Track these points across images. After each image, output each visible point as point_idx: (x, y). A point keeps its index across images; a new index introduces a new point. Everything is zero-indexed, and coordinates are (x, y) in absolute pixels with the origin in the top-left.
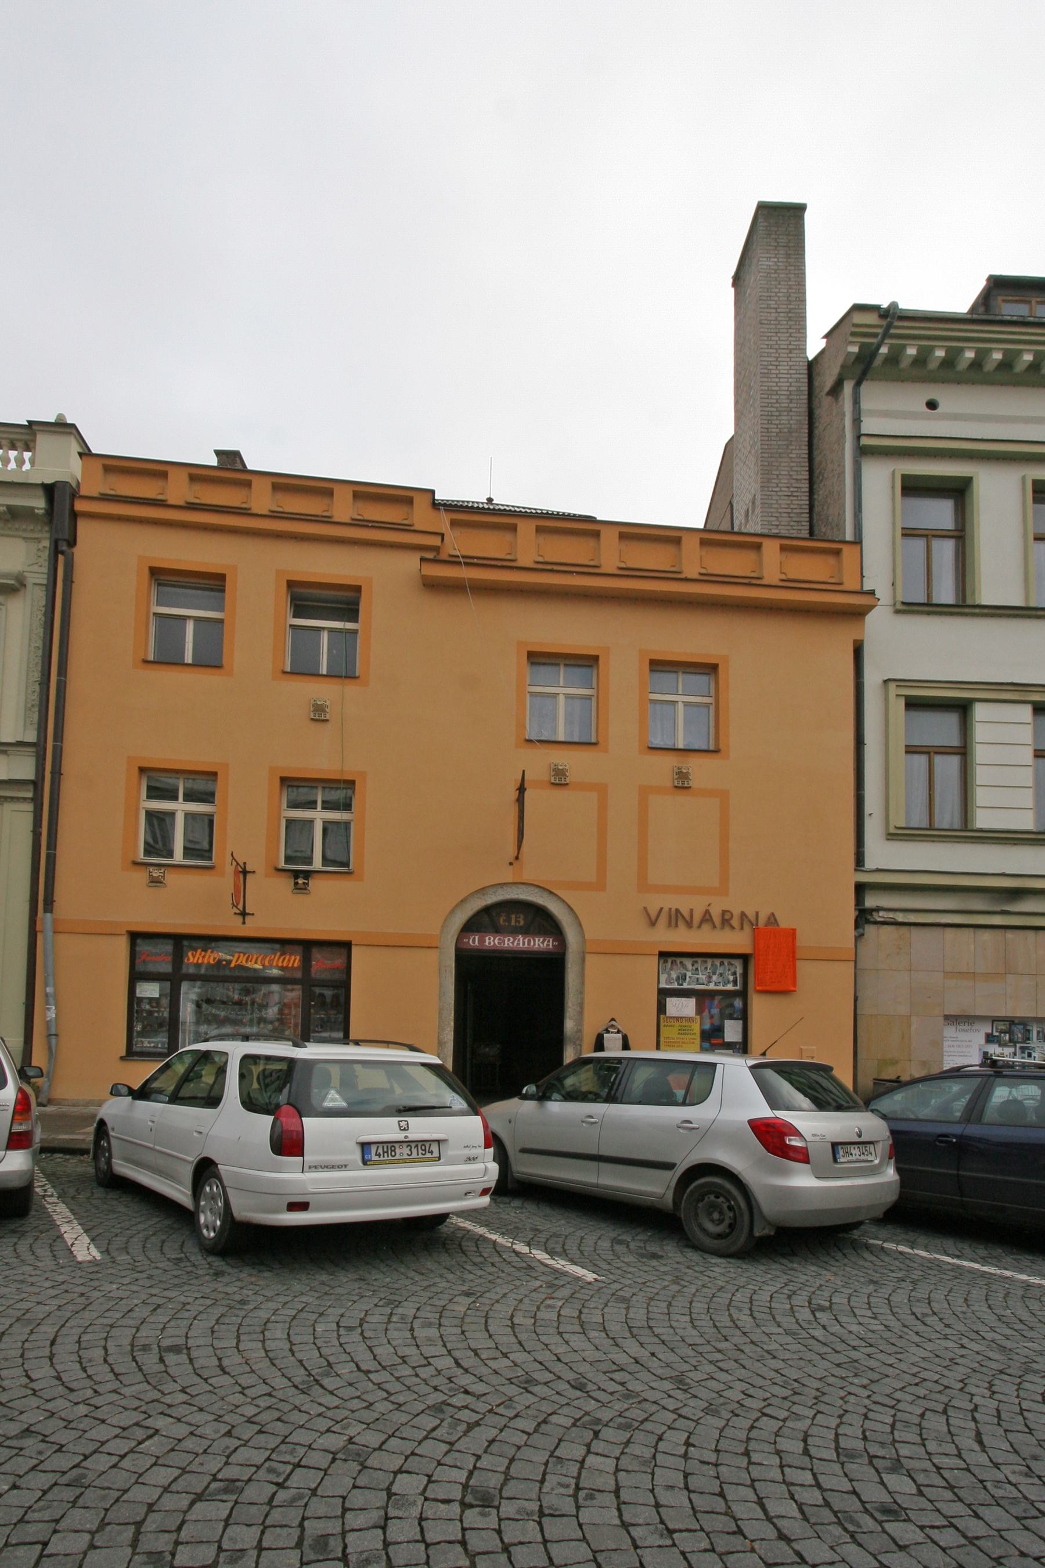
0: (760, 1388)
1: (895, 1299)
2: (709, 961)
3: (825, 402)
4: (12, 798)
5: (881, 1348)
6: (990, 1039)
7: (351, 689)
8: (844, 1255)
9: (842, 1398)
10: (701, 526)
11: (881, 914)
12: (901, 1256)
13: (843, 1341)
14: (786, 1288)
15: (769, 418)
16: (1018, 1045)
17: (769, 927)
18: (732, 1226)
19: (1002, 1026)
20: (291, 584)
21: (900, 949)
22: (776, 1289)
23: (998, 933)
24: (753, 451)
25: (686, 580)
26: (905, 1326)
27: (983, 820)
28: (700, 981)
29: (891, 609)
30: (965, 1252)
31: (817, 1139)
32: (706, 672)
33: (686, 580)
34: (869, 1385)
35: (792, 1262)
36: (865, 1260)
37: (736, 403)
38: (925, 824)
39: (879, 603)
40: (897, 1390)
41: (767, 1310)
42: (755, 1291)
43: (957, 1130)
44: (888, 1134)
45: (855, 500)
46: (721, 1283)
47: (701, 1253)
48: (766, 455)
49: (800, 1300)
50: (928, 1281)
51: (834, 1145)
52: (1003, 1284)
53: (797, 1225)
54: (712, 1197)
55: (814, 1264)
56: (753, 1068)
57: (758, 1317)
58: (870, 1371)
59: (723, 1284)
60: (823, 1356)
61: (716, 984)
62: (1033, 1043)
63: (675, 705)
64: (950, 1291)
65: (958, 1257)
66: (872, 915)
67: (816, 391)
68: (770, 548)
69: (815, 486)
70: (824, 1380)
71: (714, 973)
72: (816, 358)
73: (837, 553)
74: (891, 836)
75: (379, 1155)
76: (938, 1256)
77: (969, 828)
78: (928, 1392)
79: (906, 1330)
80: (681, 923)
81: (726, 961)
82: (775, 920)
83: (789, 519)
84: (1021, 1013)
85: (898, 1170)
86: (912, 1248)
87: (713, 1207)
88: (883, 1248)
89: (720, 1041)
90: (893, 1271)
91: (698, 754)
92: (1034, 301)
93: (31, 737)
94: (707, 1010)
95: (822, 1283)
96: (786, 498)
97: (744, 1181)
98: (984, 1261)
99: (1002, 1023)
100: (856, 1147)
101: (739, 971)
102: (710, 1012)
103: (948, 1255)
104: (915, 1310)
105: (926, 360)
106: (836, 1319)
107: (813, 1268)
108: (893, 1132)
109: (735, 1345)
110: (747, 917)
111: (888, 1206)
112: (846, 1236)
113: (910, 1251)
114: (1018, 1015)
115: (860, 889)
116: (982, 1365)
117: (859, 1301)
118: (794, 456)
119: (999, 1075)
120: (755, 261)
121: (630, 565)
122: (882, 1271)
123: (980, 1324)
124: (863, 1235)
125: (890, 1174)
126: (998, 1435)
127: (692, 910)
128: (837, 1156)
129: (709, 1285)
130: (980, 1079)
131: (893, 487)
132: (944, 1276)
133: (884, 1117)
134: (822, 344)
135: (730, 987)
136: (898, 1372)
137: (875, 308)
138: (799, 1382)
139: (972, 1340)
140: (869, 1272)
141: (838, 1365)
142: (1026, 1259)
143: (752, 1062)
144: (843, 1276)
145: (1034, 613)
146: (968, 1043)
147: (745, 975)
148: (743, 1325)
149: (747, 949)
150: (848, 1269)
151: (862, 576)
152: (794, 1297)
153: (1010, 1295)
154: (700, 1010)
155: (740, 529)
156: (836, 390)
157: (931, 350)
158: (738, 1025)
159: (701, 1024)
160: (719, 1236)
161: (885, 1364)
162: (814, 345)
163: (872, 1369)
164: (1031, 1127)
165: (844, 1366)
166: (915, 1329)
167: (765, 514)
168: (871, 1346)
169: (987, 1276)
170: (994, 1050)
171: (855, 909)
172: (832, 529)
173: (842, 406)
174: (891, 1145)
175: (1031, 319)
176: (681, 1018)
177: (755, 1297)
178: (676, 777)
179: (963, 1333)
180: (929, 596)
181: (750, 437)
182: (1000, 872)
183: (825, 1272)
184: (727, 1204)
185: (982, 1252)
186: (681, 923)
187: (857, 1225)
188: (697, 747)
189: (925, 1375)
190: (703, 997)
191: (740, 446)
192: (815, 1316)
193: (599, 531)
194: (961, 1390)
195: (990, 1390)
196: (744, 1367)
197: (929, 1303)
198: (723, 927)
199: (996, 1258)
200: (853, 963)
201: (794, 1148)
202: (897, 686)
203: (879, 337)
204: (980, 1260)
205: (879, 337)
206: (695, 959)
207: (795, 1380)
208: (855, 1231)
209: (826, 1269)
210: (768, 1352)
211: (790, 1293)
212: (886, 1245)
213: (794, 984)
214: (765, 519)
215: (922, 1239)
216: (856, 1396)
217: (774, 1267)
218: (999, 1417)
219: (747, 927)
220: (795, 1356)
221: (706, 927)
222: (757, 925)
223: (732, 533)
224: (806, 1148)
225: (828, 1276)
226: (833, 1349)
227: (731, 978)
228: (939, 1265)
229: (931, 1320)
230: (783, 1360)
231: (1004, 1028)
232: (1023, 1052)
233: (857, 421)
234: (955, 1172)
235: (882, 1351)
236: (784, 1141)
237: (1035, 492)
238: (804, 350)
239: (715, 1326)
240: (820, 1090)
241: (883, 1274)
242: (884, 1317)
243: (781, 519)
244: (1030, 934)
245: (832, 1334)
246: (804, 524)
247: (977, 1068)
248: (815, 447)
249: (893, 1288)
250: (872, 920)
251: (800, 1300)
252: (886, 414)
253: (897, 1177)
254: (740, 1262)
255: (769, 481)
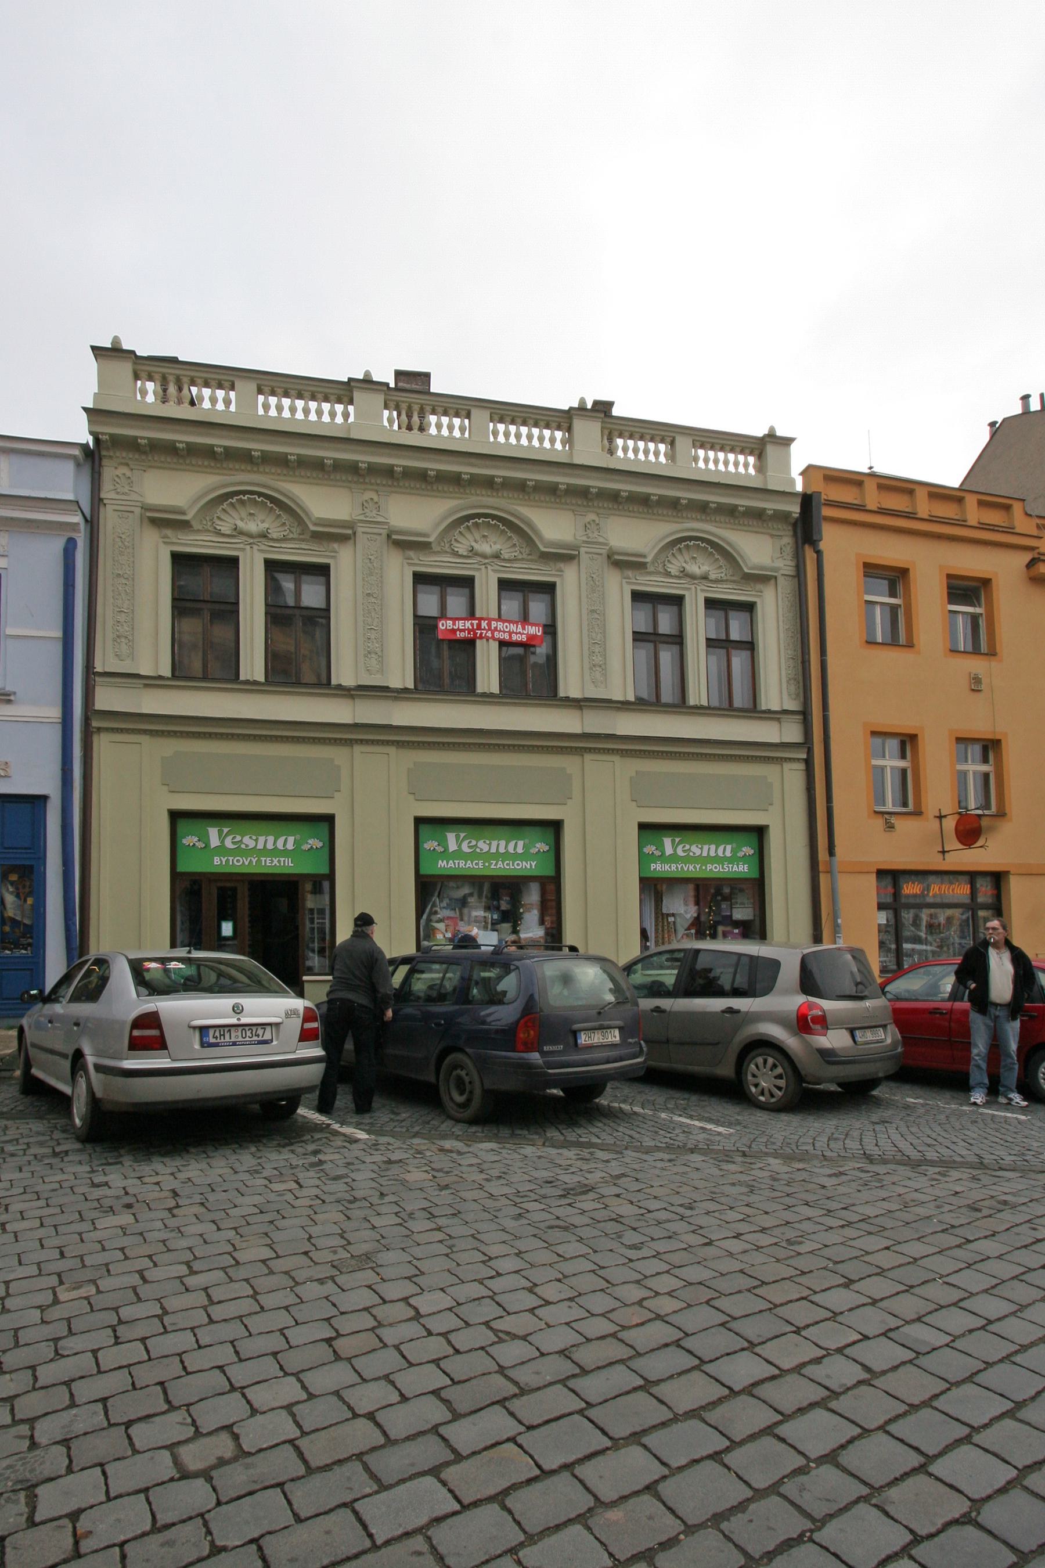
4: (790, 759)
7: (994, 664)
20: (949, 576)
75: (216, 1038)
93: (792, 705)
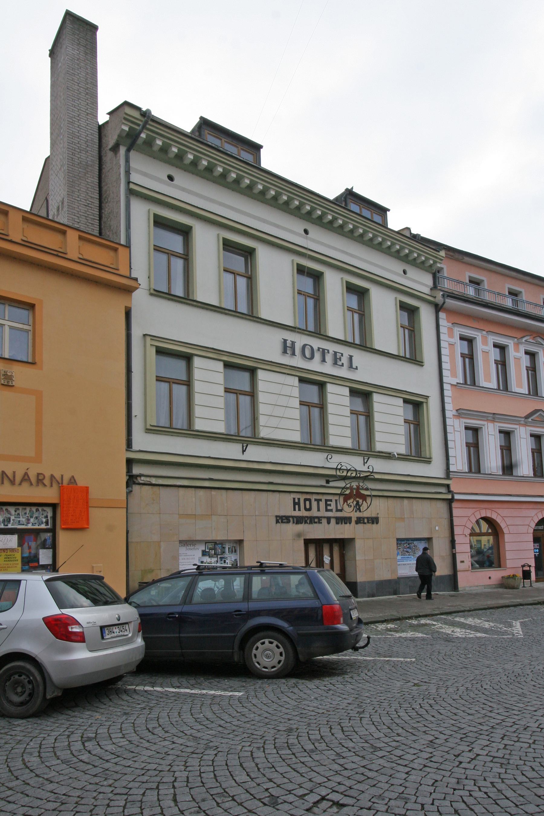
0: (37, 807)
1: (137, 722)
2: (28, 509)
3: (109, 156)
5: (124, 757)
6: (204, 553)
8: (110, 700)
9: (94, 798)
10: (28, 210)
11: (142, 478)
12: (146, 693)
13: (101, 758)
14: (68, 730)
15: (73, 152)
16: (219, 556)
17: (71, 485)
18: (31, 695)
19: (210, 546)
21: (154, 500)
22: (59, 733)
23: (208, 491)
24: (62, 170)
25: (11, 241)
26: (141, 738)
27: (199, 425)
28: (21, 522)
29: (148, 292)
30: (183, 683)
31: (90, 625)
32: (28, 308)
33: (11, 241)
34: (113, 783)
35: (74, 712)
36: (123, 700)
37: (52, 134)
38: (168, 425)
39: (140, 287)
40: (130, 782)
41: (52, 750)
42: (45, 737)
43: (178, 609)
44: (138, 616)
45: (126, 221)
46: (19, 738)
47: (7, 719)
48: (71, 175)
49: (76, 737)
50: (159, 706)
51: (102, 628)
52: (201, 699)
53: (80, 685)
54: (16, 677)
55: (89, 710)
56: (47, 581)
57: (43, 757)
58: (116, 774)
59: (22, 738)
60: (86, 772)
61: (33, 525)
62: (227, 555)
63: (2, 327)
64: (171, 710)
65: (178, 687)
66: (137, 479)
67: (104, 145)
68: (72, 236)
69: (103, 205)
70: (84, 788)
71: (32, 517)
72: (104, 125)
73: (116, 250)
74: (148, 431)
76: (167, 689)
77: (192, 429)
78: (149, 778)
79: (141, 740)
80: (6, 481)
81: (40, 509)
82: (75, 480)
83: (86, 221)
84: (220, 537)
85: (144, 639)
86: (153, 687)
87: (17, 683)
88: (135, 690)
89: (36, 564)
90: (139, 704)
91: (20, 364)
92: (223, 140)
94: (26, 544)
95: (93, 721)
96: (84, 206)
97: (39, 661)
98: (193, 687)
99: (210, 544)
100: (117, 627)
101: (50, 514)
102: (28, 544)
103: (174, 687)
104: (148, 726)
105: (226, 176)
106: (98, 744)
107: (88, 713)
108: (141, 615)
109: (24, 781)
110: (55, 478)
111: (139, 662)
112: (114, 687)
113: (152, 689)
114: (218, 539)
115: (130, 462)
116: (183, 752)
117: (115, 728)
118: (90, 181)
119: (201, 574)
120: (64, 47)
121: (86, 257)
122: (132, 705)
123: (186, 726)
124: (124, 684)
125: (139, 642)
126: (186, 792)
127: (14, 473)
128: (104, 635)
129: (10, 741)
130: (190, 578)
131: (149, 219)
132: (169, 701)
133: (137, 606)
134: (107, 118)
135: (43, 526)
136: (133, 769)
137: (138, 109)
138: (66, 795)
139: (179, 737)
140: (124, 708)
141: (95, 776)
142: (215, 681)
143: (46, 577)
144: (107, 714)
145: (223, 311)
146: (193, 557)
147: (54, 518)
148: (32, 765)
149: (55, 501)
150: (111, 708)
151: (131, 268)
152: (72, 736)
153: (204, 704)
154: (21, 543)
155: (54, 218)
156: (115, 149)
157: (242, 177)
158: (49, 552)
159: (22, 553)
160: (22, 704)
161: (125, 766)
162: (103, 118)
163: (117, 772)
164: (214, 603)
165: (99, 775)
166: (147, 739)
167: (70, 213)
168: (118, 756)
169: (193, 696)
170: (206, 559)
171: (127, 475)
172: (113, 234)
173: (119, 159)
174: (140, 624)
175: (222, 149)
176: (7, 549)
177: (43, 742)
178: (2, 377)
179: (175, 734)
180: (169, 288)
181: (61, 159)
182: (207, 456)
183: (96, 714)
184: (28, 679)
185: (192, 681)
186: (6, 481)
187: (119, 678)
188: (19, 359)
189: (149, 767)
190: (22, 534)
191: (54, 163)
192: (84, 746)
193: (118, 248)
194: (169, 771)
195: (185, 766)
196: (28, 796)
197: (158, 720)
198: (38, 485)
199: (199, 683)
200: (125, 509)
201: (75, 633)
202: (151, 339)
203: (141, 127)
204: (191, 687)
205: (141, 127)
206: (17, 507)
207: (64, 795)
208: (119, 682)
209: (97, 712)
210: (47, 779)
211: (69, 733)
212: (137, 688)
213: (88, 523)
214: (70, 216)
215: (160, 680)
216: (104, 793)
217: (60, 718)
218: (188, 781)
219: (55, 485)
220: (67, 777)
221: (25, 485)
222: (62, 483)
223: (47, 219)
224: (83, 633)
225: (97, 716)
226: (93, 765)
227: (44, 520)
228: (166, 695)
229: (157, 731)
230: (57, 783)
231: (211, 546)
232: (221, 560)
233: (128, 173)
234: (178, 635)
235: (125, 758)
236: (67, 629)
237: (224, 244)
238: (96, 117)
239: (10, 771)
240: (98, 594)
241: (133, 707)
242: (129, 735)
243: (80, 219)
244: (224, 492)
245: (94, 755)
246: (95, 226)
247: (195, 570)
248: (103, 180)
249: (137, 715)
250: (137, 482)
251: (76, 737)
252: (145, 174)
253: (143, 643)
254: (37, 719)
255: (73, 192)
